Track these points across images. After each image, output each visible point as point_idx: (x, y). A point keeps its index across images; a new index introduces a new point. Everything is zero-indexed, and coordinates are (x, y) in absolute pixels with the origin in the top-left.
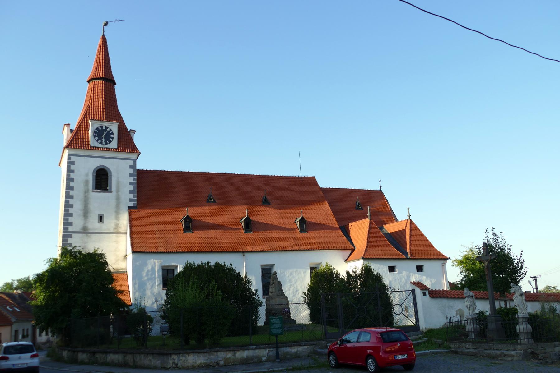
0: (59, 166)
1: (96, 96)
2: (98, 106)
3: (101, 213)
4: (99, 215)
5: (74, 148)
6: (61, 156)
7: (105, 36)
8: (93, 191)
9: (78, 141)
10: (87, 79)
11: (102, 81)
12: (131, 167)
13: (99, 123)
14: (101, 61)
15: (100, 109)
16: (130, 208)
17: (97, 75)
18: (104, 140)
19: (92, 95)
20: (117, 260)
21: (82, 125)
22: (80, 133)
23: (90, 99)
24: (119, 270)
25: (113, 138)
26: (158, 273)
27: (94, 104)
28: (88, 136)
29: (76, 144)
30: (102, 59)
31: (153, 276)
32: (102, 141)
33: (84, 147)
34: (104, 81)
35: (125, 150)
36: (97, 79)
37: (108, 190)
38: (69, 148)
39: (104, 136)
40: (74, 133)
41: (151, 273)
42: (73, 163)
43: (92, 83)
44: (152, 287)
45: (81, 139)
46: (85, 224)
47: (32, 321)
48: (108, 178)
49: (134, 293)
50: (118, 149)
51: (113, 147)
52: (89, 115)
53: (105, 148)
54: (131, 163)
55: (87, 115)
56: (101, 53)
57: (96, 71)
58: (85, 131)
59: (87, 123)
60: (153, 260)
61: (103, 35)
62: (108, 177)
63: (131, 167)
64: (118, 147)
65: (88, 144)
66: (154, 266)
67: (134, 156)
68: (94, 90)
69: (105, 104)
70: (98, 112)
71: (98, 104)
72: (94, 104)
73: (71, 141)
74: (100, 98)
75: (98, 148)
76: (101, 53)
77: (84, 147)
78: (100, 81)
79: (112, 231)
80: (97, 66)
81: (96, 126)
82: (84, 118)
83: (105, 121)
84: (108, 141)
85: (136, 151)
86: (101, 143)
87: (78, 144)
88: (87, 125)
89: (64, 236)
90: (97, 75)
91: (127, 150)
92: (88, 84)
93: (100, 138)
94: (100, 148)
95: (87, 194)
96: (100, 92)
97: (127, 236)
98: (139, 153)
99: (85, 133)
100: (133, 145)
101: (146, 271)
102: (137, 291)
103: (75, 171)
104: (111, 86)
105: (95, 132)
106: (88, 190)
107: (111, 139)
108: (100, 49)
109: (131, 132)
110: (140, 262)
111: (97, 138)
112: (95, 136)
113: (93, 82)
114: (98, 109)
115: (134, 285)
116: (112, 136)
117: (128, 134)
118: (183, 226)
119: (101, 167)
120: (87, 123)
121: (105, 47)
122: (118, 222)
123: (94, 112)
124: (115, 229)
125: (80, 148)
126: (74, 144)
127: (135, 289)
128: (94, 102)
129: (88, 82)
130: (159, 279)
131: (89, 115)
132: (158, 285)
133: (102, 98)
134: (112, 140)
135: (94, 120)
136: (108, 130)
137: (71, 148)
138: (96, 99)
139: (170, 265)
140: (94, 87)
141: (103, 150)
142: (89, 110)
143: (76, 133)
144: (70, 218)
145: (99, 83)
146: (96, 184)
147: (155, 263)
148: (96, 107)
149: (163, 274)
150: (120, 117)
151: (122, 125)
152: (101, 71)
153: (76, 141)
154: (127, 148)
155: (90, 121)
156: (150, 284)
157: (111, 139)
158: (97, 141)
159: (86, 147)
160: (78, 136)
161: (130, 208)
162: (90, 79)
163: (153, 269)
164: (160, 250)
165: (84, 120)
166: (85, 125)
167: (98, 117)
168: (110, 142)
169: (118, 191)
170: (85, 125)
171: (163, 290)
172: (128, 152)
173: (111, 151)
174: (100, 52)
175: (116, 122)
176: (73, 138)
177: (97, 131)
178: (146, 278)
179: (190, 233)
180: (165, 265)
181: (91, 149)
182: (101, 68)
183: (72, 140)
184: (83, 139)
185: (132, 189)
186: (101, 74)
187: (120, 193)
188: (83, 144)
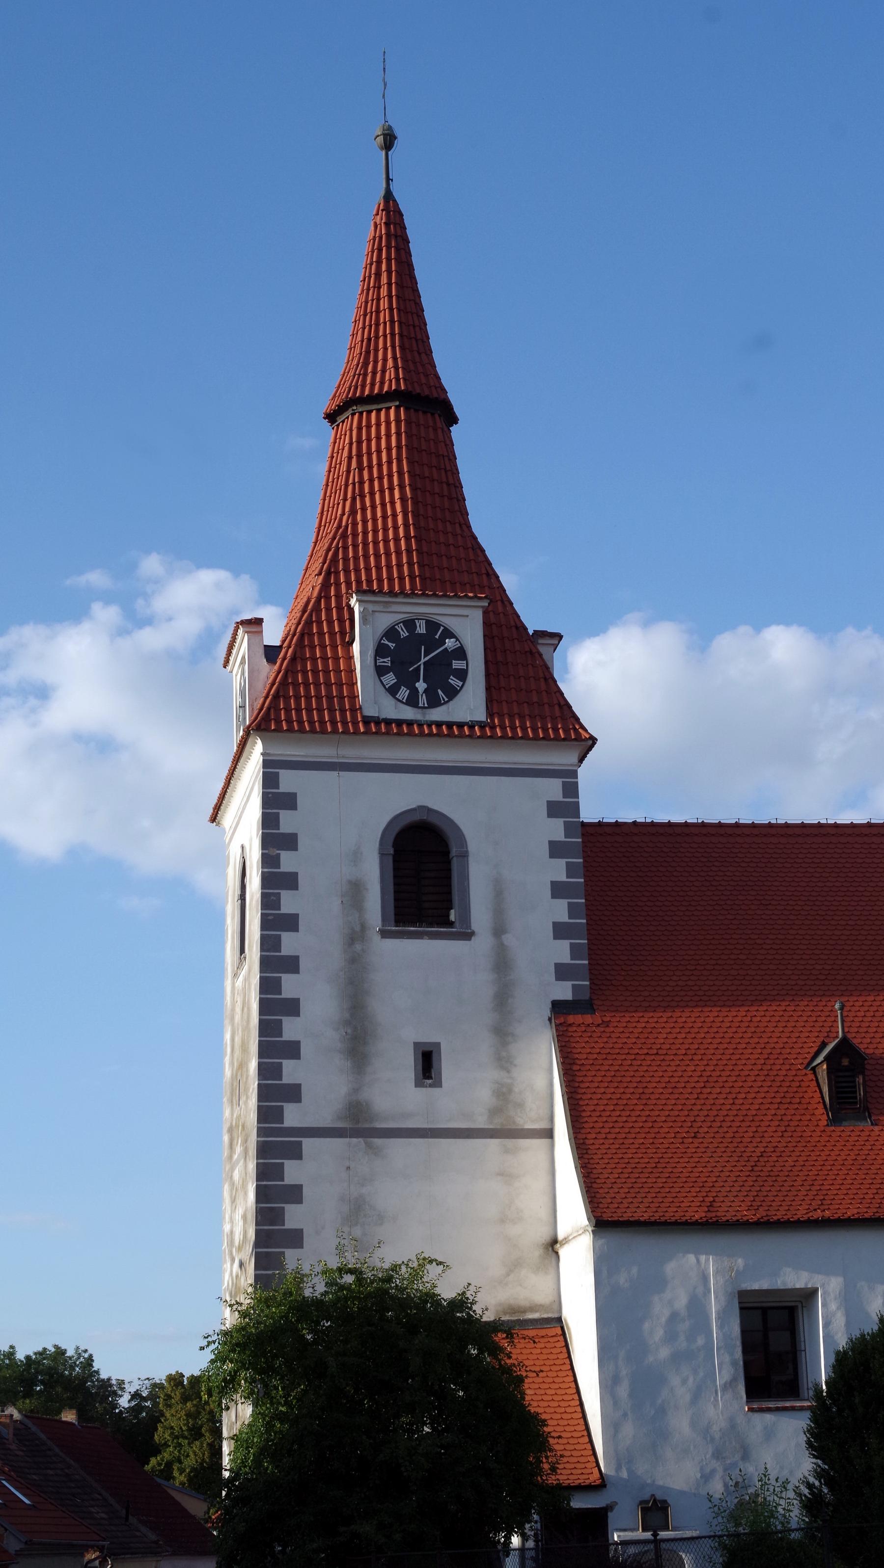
0: (214, 819)
1: (371, 480)
2: (385, 530)
3: (428, 1037)
4: (416, 1045)
5: (290, 730)
6: (225, 773)
7: (395, 201)
8: (385, 934)
9: (308, 698)
10: (325, 404)
11: (398, 408)
12: (554, 809)
13: (395, 608)
14: (384, 316)
15: (397, 540)
16: (558, 1007)
17: (373, 384)
18: (421, 686)
19: (354, 476)
20: (514, 1266)
21: (319, 623)
22: (314, 659)
23: (345, 500)
24: (524, 1311)
25: (462, 675)
26: (720, 1327)
27: (365, 521)
28: (351, 671)
29: (299, 710)
30: (391, 309)
31: (700, 1341)
32: (414, 692)
33: (334, 722)
34: (406, 409)
35: (524, 729)
36: (372, 399)
37: (451, 924)
38: (267, 729)
39: (423, 661)
40: (284, 659)
41: (687, 1323)
42: (289, 801)
43: (350, 421)
44: (696, 1397)
45: (317, 685)
46: (356, 1090)
47: (86, 1548)
48: (449, 870)
49: (611, 1426)
50: (493, 728)
51: (467, 717)
52: (347, 571)
53: (430, 726)
54: (553, 789)
55: (337, 573)
56: (384, 279)
57: (366, 364)
58: (334, 647)
59: (339, 608)
60: (691, 1258)
61: (388, 196)
62: (449, 862)
63: (554, 809)
64: (490, 714)
65: (354, 710)
66: (700, 1290)
67: (563, 758)
68: (359, 456)
69: (416, 515)
70: (388, 554)
71: (385, 517)
72: (365, 521)
73: (276, 697)
74: (391, 489)
75: (399, 723)
76: (384, 279)
77: (334, 722)
78: (389, 408)
79: (481, 1122)
80: (369, 339)
81: (385, 621)
82: (325, 586)
83: (424, 595)
84: (440, 692)
85: (575, 729)
86: (412, 701)
87: (309, 710)
88: (341, 621)
89: (263, 1150)
90: (373, 384)
91: (535, 730)
92: (328, 432)
93: (407, 679)
94: (410, 723)
95: (358, 947)
96: (390, 462)
97: (552, 1146)
98: (591, 742)
99: (336, 659)
100: (559, 705)
101: (663, 1320)
102: (625, 1415)
103: (303, 842)
104: (435, 430)
105: (380, 651)
106: (363, 927)
107: (454, 681)
108: (379, 262)
109: (541, 641)
110: (635, 1270)
111: (390, 679)
112: (380, 671)
113: (356, 417)
114: (386, 541)
115: (608, 1385)
116: (457, 664)
117: (531, 653)
118: (825, 1089)
119: (417, 817)
120: (339, 608)
121: (397, 249)
122: (509, 1081)
123: (366, 557)
124: (495, 1112)
125: (318, 730)
126: (288, 710)
127: (616, 1403)
128: (364, 509)
129: (331, 417)
130: (727, 1358)
131: (347, 571)
132: (725, 1387)
133: (402, 487)
134: (460, 684)
135: (371, 592)
136: (450, 643)
137: (279, 729)
138: (372, 493)
139: (779, 1284)
140: (359, 442)
141: (422, 734)
142: (346, 548)
143: (294, 659)
144: (288, 1065)
145: (383, 418)
146: (396, 900)
147: (705, 1278)
148: (375, 531)
149: (745, 1332)
150: (488, 574)
151: (500, 609)
152: (390, 363)
153: (297, 698)
154: (532, 718)
155: (353, 601)
156: (684, 1381)
157: (454, 681)
158: (393, 691)
159: (345, 723)
160: (305, 672)
161: (558, 1007)
162: (337, 402)
163: (697, 1306)
164: (727, 1211)
165: (328, 598)
166: (330, 623)
167: (391, 579)
168: (452, 693)
169: (499, 931)
170: (330, 623)
171: (751, 1410)
172: (536, 738)
173: (564, 740)
174: (378, 275)
175: (476, 597)
176: (284, 683)
177: (392, 645)
178: (664, 1353)
179: (862, 1125)
180: (756, 1286)
181: (367, 732)
182: (385, 349)
183: (277, 691)
184: (328, 685)
185: (563, 917)
186: (390, 374)
187: (508, 939)
188: (332, 711)
